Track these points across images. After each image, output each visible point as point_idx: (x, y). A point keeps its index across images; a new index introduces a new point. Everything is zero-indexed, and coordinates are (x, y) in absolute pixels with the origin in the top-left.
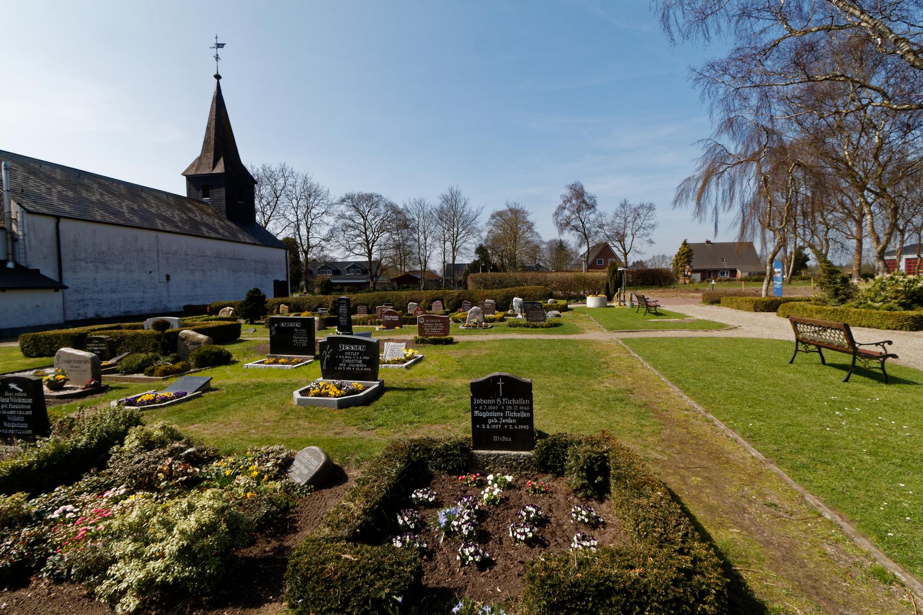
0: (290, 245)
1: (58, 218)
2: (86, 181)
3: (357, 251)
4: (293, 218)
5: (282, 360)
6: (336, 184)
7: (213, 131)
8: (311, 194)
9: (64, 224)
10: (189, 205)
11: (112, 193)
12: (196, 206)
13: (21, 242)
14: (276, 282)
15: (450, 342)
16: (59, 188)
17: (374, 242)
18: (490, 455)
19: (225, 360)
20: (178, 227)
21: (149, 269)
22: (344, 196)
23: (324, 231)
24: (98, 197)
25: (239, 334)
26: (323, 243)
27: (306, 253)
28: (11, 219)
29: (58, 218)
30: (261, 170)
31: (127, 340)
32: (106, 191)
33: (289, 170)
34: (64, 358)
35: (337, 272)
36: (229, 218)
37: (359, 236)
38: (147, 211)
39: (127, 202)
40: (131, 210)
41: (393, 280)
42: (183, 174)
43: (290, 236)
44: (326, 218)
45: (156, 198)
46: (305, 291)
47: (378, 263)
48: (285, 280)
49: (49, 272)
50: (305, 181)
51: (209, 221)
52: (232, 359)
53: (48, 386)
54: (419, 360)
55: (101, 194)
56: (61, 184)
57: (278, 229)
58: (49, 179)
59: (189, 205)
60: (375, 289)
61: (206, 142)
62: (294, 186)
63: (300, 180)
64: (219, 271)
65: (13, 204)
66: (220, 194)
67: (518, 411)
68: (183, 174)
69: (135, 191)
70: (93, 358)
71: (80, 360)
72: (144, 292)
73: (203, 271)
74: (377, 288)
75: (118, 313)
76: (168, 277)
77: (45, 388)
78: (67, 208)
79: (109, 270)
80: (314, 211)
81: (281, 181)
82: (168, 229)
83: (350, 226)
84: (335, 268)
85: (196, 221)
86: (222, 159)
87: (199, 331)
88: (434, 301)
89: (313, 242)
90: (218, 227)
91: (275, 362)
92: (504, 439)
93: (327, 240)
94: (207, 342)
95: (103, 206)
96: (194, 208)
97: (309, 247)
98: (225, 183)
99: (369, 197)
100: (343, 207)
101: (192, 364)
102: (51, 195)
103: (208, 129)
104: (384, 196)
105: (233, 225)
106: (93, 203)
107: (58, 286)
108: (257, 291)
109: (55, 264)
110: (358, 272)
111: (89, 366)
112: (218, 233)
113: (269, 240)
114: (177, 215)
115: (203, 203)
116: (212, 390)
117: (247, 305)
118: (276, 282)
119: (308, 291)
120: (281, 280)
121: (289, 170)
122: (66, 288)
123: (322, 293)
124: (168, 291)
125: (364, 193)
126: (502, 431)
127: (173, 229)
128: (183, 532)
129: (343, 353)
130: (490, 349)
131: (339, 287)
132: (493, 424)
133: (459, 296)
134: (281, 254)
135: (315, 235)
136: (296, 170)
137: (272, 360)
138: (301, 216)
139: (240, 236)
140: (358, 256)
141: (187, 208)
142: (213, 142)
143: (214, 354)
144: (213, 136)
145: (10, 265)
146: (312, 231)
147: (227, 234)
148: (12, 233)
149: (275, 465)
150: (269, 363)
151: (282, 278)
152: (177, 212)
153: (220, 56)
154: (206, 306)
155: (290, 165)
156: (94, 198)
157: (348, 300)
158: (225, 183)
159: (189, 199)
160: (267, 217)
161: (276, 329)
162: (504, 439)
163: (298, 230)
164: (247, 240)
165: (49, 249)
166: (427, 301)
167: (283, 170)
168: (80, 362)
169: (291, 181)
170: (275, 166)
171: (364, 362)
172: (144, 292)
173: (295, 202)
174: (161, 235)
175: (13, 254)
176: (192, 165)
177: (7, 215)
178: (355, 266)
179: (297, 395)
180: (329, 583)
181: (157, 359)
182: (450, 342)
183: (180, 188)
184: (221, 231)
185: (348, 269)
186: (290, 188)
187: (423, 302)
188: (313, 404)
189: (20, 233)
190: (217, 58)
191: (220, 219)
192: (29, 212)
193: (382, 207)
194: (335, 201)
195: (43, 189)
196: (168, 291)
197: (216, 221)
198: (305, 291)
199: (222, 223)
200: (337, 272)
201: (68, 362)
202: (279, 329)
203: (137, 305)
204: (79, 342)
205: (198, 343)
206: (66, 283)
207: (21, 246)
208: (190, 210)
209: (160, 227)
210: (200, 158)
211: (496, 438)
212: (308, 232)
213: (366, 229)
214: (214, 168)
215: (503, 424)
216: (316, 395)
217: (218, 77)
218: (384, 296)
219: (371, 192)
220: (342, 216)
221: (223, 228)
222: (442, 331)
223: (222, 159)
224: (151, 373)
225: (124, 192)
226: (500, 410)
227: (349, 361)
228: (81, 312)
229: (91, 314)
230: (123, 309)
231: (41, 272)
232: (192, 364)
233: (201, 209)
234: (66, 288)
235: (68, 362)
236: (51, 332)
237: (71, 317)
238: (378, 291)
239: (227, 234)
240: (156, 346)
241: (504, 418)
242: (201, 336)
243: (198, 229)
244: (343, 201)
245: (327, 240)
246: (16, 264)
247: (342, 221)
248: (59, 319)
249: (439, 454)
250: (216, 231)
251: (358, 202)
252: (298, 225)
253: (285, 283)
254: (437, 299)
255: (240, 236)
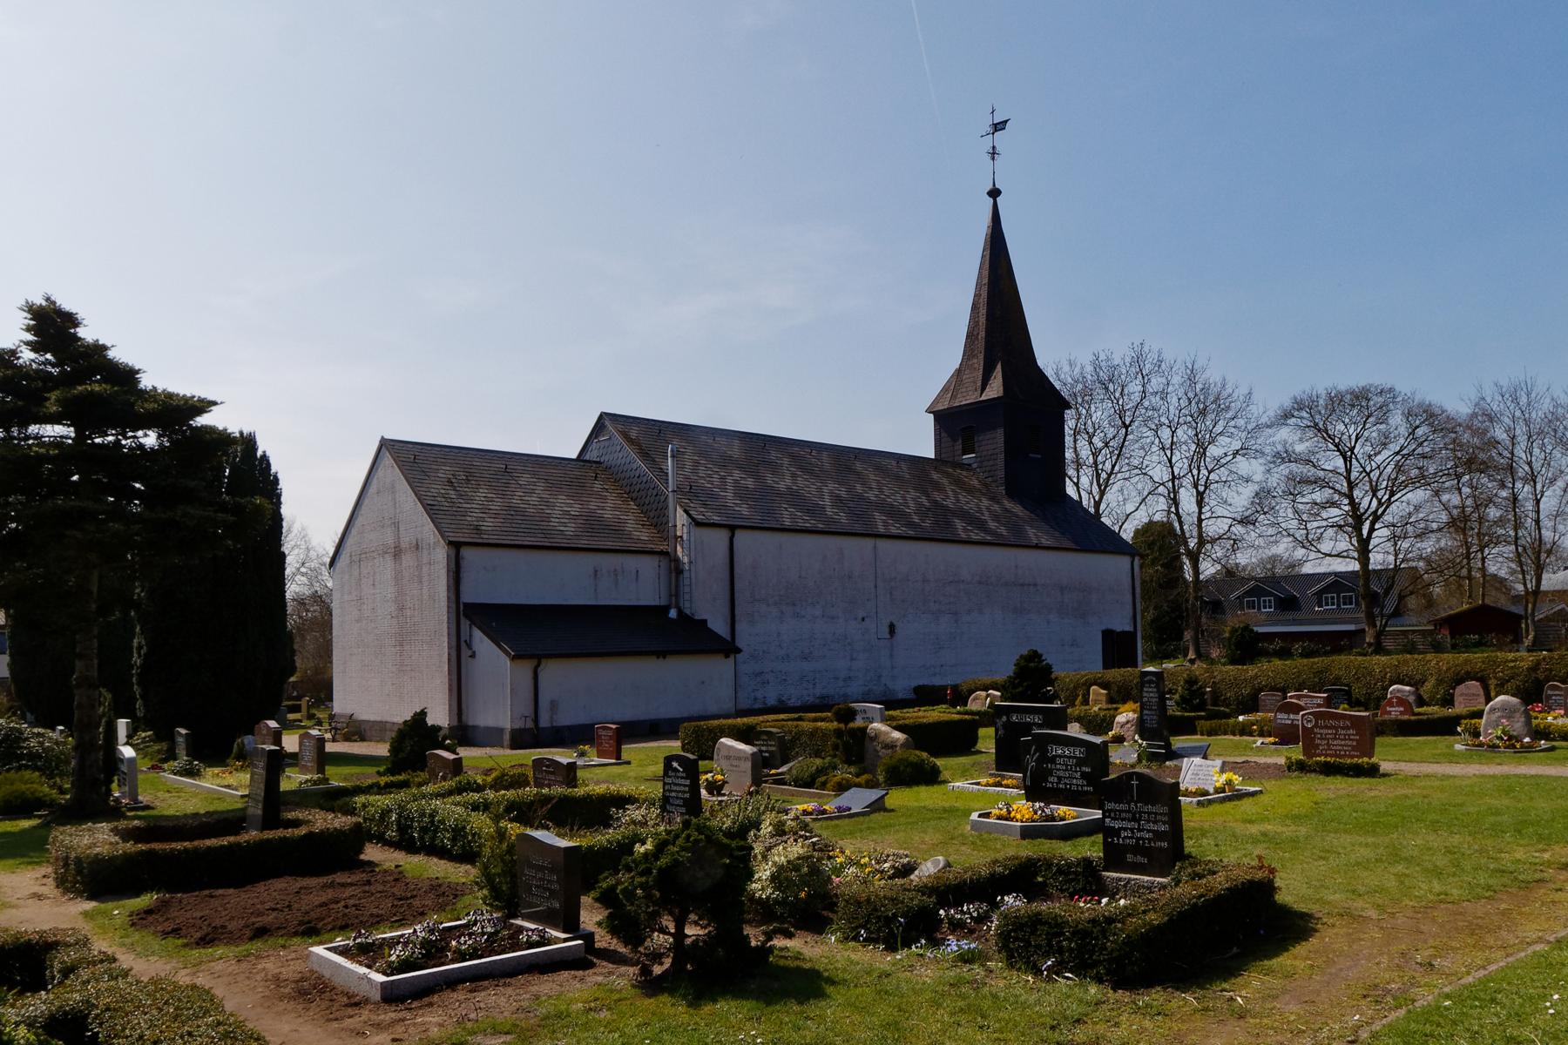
0: (1162, 545)
1: (732, 529)
2: (774, 455)
3: (1326, 547)
4: (1160, 473)
5: (1009, 782)
6: (1268, 378)
7: (983, 311)
8: (1206, 407)
9: (742, 537)
10: (935, 476)
11: (807, 469)
12: (948, 475)
13: (686, 574)
14: (1108, 635)
15: (1373, 771)
16: (737, 474)
17: (1376, 518)
18: (1120, 879)
19: (931, 777)
20: (911, 525)
21: (861, 614)
22: (1288, 403)
23: (1241, 499)
24: (788, 481)
25: (975, 743)
26: (1238, 530)
27: (1195, 558)
28: (676, 537)
29: (732, 529)
30: (1089, 369)
31: (804, 739)
32: (801, 468)
33: (1152, 358)
34: (724, 752)
35: (1288, 604)
36: (1011, 494)
37: (1333, 504)
38: (861, 498)
39: (832, 486)
40: (837, 500)
41: (1440, 623)
42: (928, 411)
43: (1157, 518)
44: (1243, 466)
45: (879, 469)
46: (1191, 655)
47: (1390, 576)
48: (1129, 628)
49: (719, 626)
50: (1191, 379)
51: (969, 503)
52: (942, 778)
53: (707, 788)
54: (1240, 796)
55: (794, 476)
56: (740, 468)
57: (1128, 508)
58: (726, 462)
59: (935, 476)
60: (1379, 649)
61: (971, 336)
62: (1164, 395)
63: (1176, 380)
64: (981, 610)
65: (680, 511)
66: (995, 441)
67: (1155, 822)
68: (928, 411)
69: (846, 461)
70: (753, 754)
71: (739, 756)
72: (852, 659)
73: (956, 614)
74: (1388, 644)
75: (811, 699)
76: (892, 629)
77: (703, 792)
78: (744, 510)
79: (808, 609)
80: (1213, 451)
81: (1135, 388)
82: (894, 531)
83: (1306, 481)
84: (1281, 590)
85: (946, 509)
86: (999, 367)
87: (897, 728)
88: (1460, 681)
89: (1213, 528)
90: (986, 516)
91: (999, 784)
92: (1140, 859)
93: (1245, 521)
94: (905, 745)
95: (795, 498)
96: (945, 481)
97: (1202, 541)
98: (1010, 414)
99: (1360, 398)
100: (1285, 434)
101: (881, 778)
102: (725, 490)
103: (975, 307)
104: (1403, 387)
105: (1017, 509)
106: (780, 494)
107: (728, 648)
108: (1035, 656)
109: (727, 611)
110: (1348, 601)
111: (749, 764)
112: (987, 531)
113: (1087, 532)
114: (909, 500)
115: (962, 466)
116: (886, 810)
117: (1015, 687)
118: (1108, 635)
119: (1199, 655)
120: (1119, 629)
121: (1152, 358)
122: (739, 651)
123: (1233, 662)
124: (891, 656)
125: (1342, 387)
126: (1138, 849)
127: (903, 530)
128: (775, 863)
129: (1053, 760)
130: (1424, 788)
131: (1278, 644)
132: (1126, 838)
133: (1535, 668)
134: (1119, 566)
135: (1220, 511)
136: (1168, 356)
137: (991, 781)
138: (1181, 466)
139: (1031, 532)
140: (1331, 557)
141: (932, 482)
142: (982, 334)
143: (911, 764)
144: (982, 320)
145: (673, 614)
146: (1211, 500)
147: (1003, 531)
148: (677, 560)
149: (893, 867)
150: (988, 785)
151: (1122, 624)
152: (913, 492)
153: (998, 149)
154: (945, 688)
155: (1153, 347)
156: (782, 486)
157: (1159, 675)
158: (1010, 414)
159: (939, 462)
160: (1104, 475)
161: (1005, 726)
162: (1140, 859)
163: (1176, 502)
164: (1044, 542)
165: (721, 589)
166: (1440, 682)
167: (1138, 360)
168: (739, 759)
169: (1156, 383)
170: (1119, 352)
171: (1084, 775)
172: (852, 659)
173: (1165, 433)
174: (883, 544)
175: (677, 595)
176: (945, 389)
177: (671, 533)
178: (1337, 584)
179: (974, 816)
180: (858, 904)
181: (835, 768)
182: (1373, 771)
183: (923, 444)
184: (992, 525)
185: (1319, 593)
186: (1156, 400)
187: (1428, 686)
188: (991, 829)
189: (686, 560)
190: (993, 153)
191: (993, 499)
192: (698, 524)
193: (1397, 419)
194: (1264, 420)
195: (716, 480)
196: (891, 656)
197: (985, 502)
198: (1191, 655)
199: (996, 507)
200: (1288, 604)
201: (728, 758)
202: (1009, 726)
203: (841, 683)
204: (745, 735)
205: (891, 746)
206: (740, 643)
207: (687, 582)
208: (937, 486)
209: (881, 530)
210: (959, 372)
211: (1130, 858)
212: (1200, 503)
213: (1351, 486)
214: (983, 389)
215: (1138, 839)
216: (999, 818)
217: (994, 193)
218: (1326, 670)
219: (1362, 383)
220: (1285, 456)
221: (996, 518)
222: (1354, 748)
223: (999, 367)
224: (823, 786)
225: (827, 466)
226: (1134, 819)
227: (1061, 774)
228: (759, 694)
229: (772, 702)
230: (818, 691)
231: (710, 625)
232: (881, 778)
233: (958, 482)
234: (739, 651)
235: (728, 758)
236: (716, 722)
237: (744, 704)
238: (1388, 653)
239: (1003, 531)
240: (836, 747)
241: (1139, 830)
242: (897, 735)
243: (949, 525)
244: (1287, 415)
245: (1245, 521)
246: (680, 612)
247: (1284, 469)
248: (729, 706)
249: (1060, 871)
250: (982, 525)
251: (1332, 414)
252: (1175, 492)
253: (1130, 637)
254: (1469, 676)
255: (1031, 532)
